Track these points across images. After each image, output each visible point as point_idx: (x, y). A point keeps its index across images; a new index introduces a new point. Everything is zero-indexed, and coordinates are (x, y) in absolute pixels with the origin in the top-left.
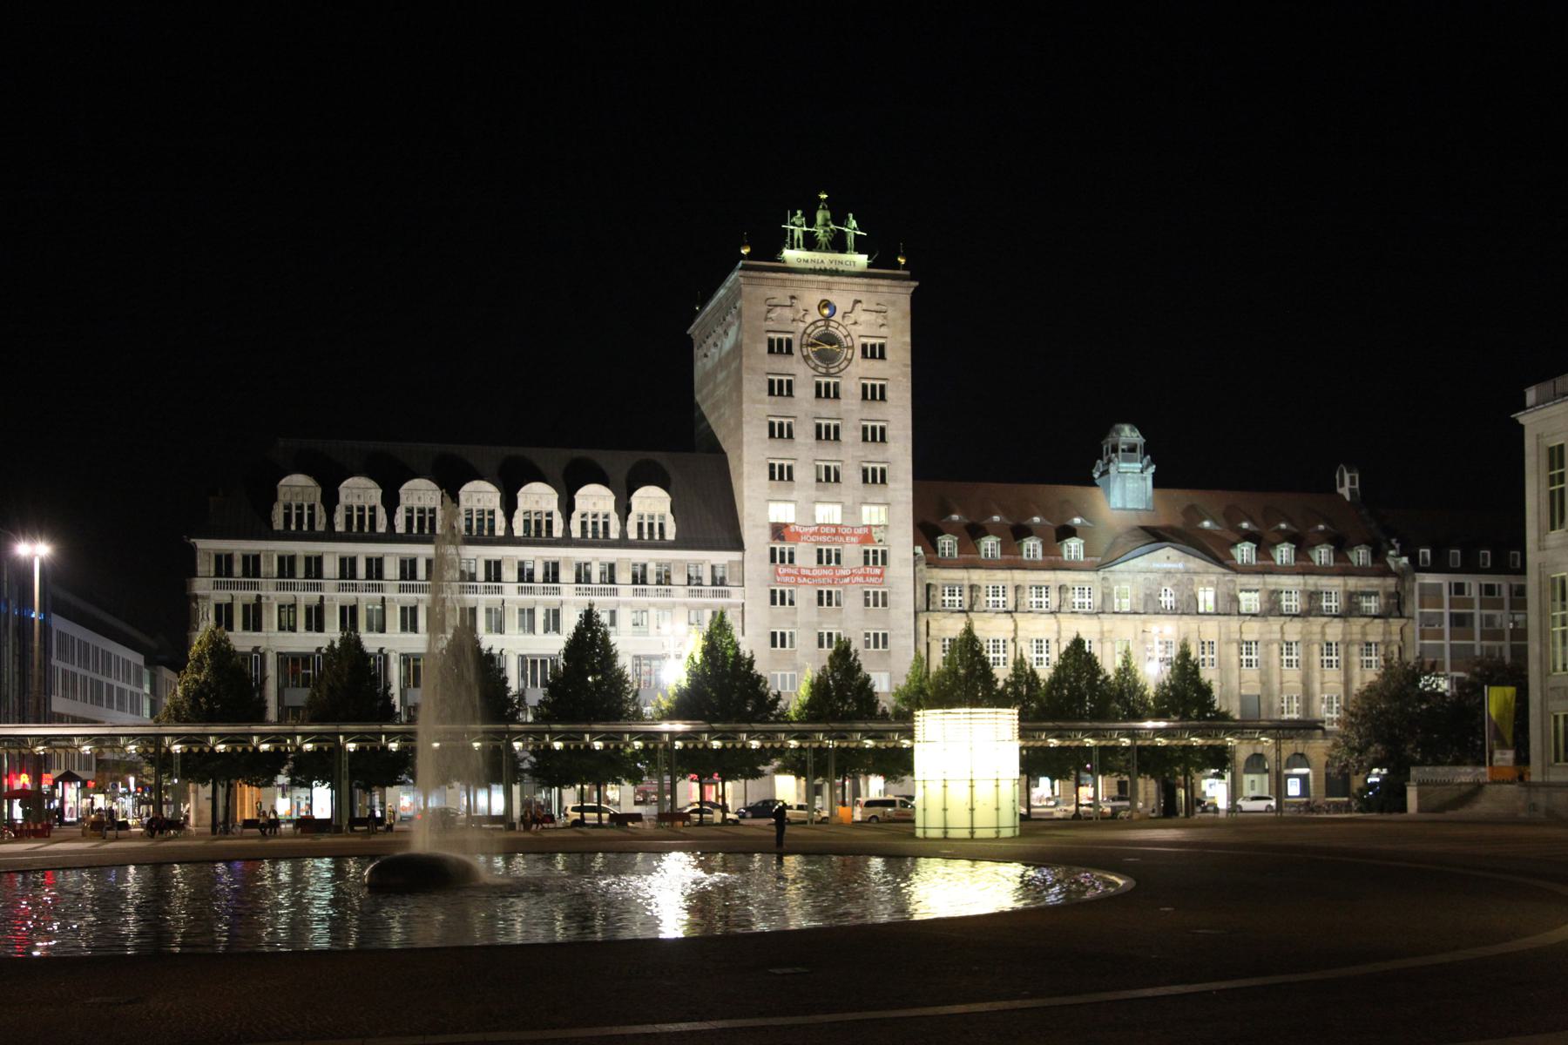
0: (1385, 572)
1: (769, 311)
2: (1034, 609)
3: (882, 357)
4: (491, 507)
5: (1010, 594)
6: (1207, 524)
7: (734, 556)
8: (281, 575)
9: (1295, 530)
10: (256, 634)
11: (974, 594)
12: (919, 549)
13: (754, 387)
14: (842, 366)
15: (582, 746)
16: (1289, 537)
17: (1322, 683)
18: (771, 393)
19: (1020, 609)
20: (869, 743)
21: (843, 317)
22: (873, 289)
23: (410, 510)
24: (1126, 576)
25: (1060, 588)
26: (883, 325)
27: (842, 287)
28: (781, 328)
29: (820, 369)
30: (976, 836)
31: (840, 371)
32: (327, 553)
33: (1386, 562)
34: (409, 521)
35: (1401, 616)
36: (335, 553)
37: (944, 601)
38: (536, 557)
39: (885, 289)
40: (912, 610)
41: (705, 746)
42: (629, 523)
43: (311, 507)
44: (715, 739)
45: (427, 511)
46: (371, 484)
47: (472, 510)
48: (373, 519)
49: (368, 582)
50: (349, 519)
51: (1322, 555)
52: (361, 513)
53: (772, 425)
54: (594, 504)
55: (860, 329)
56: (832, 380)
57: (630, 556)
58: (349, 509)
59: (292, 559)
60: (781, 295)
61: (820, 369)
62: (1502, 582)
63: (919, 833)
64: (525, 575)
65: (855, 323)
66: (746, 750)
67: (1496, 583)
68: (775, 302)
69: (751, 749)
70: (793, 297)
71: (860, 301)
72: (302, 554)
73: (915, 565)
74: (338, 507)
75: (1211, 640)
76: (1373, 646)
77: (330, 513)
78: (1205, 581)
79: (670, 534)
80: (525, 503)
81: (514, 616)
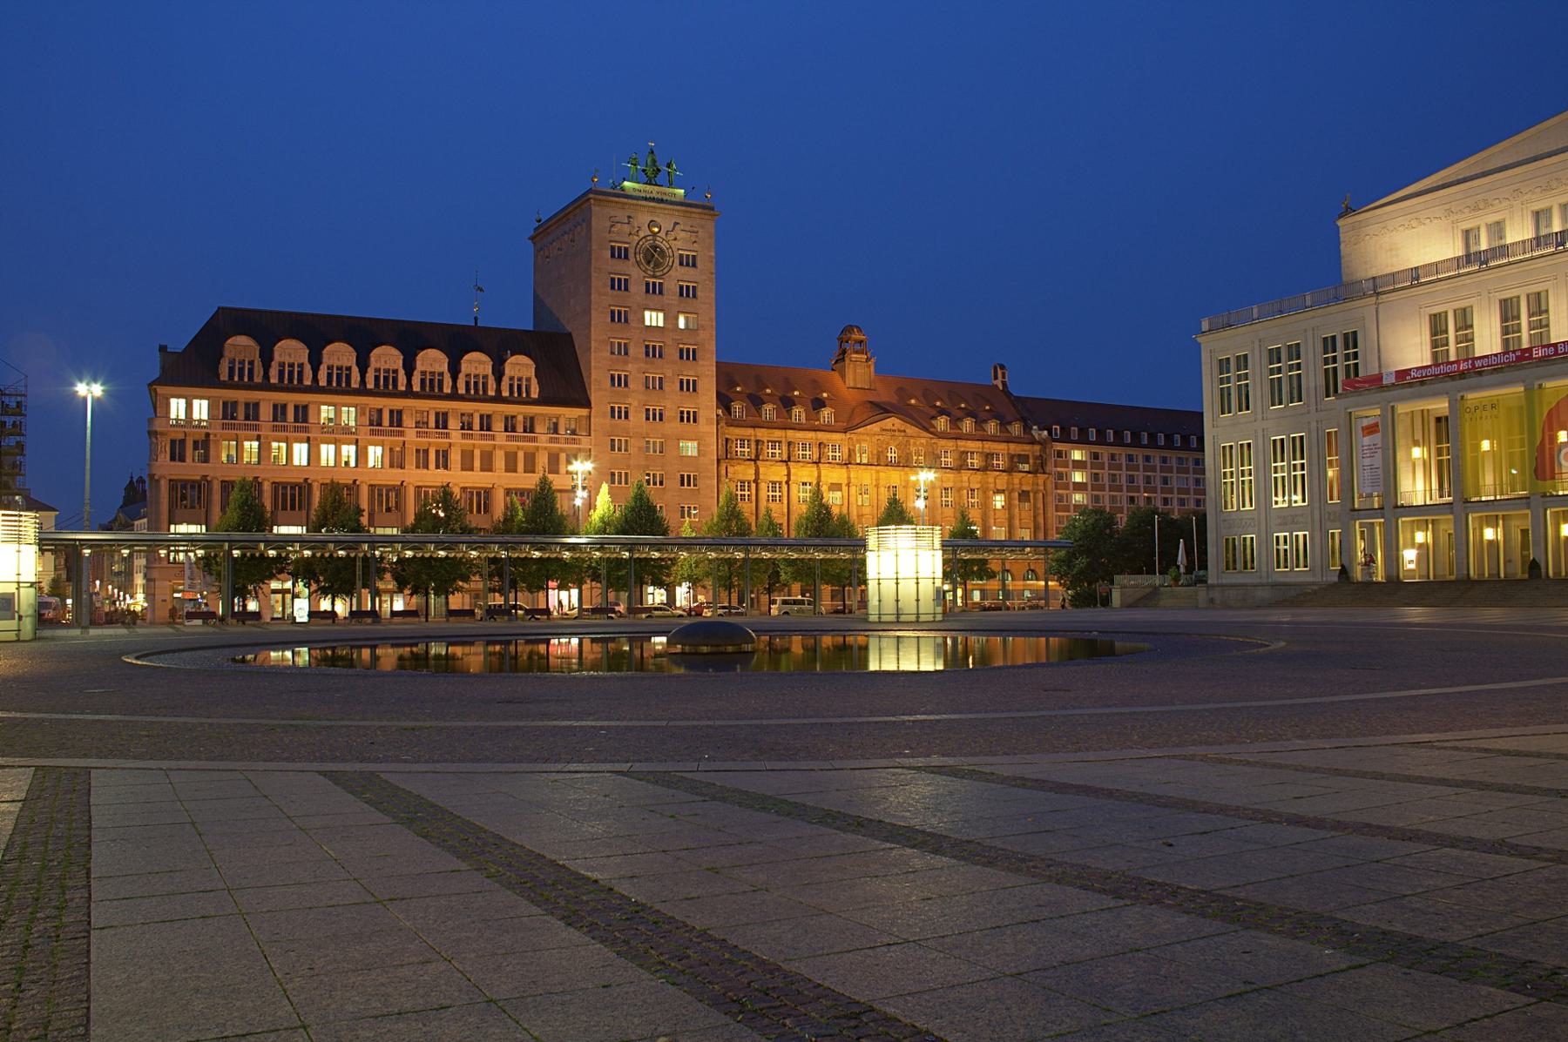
0: (1033, 442)
1: (612, 226)
2: (801, 459)
3: (694, 265)
4: (441, 370)
5: (816, 450)
6: (913, 401)
7: (584, 412)
8: (225, 417)
9: (945, 406)
10: (180, 464)
11: (759, 447)
12: (720, 412)
13: (599, 283)
14: (665, 271)
15: (257, 555)
16: (970, 414)
17: (1020, 520)
18: (613, 287)
19: (792, 459)
20: (537, 554)
21: (666, 234)
22: (688, 215)
23: (330, 368)
24: (865, 437)
25: (820, 444)
26: (695, 242)
27: (666, 212)
28: (621, 239)
29: (649, 272)
30: (921, 620)
31: (664, 274)
32: (263, 400)
33: (1032, 435)
34: (330, 376)
35: (1044, 473)
36: (270, 400)
37: (737, 451)
38: (430, 408)
39: (697, 216)
40: (715, 458)
41: (331, 555)
42: (503, 383)
43: (251, 363)
44: (408, 550)
45: (344, 369)
46: (301, 345)
47: (284, 363)
48: (300, 374)
49: (436, 430)
50: (281, 373)
51: (992, 427)
52: (291, 369)
53: (613, 312)
54: (476, 368)
55: (679, 244)
56: (658, 281)
57: (415, 405)
58: (282, 365)
59: (235, 404)
60: (621, 215)
61: (649, 272)
62: (1190, 457)
63: (873, 618)
64: (510, 425)
65: (675, 239)
66: (263, 557)
67: (1169, 456)
68: (617, 219)
69: (268, 557)
70: (629, 217)
71: (678, 223)
72: (243, 400)
73: (718, 424)
74: (415, 373)
75: (894, 485)
76: (778, 484)
77: (267, 368)
78: (918, 443)
79: (535, 395)
80: (422, 365)
81: (413, 455)
